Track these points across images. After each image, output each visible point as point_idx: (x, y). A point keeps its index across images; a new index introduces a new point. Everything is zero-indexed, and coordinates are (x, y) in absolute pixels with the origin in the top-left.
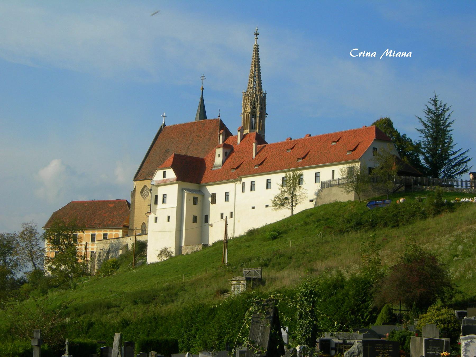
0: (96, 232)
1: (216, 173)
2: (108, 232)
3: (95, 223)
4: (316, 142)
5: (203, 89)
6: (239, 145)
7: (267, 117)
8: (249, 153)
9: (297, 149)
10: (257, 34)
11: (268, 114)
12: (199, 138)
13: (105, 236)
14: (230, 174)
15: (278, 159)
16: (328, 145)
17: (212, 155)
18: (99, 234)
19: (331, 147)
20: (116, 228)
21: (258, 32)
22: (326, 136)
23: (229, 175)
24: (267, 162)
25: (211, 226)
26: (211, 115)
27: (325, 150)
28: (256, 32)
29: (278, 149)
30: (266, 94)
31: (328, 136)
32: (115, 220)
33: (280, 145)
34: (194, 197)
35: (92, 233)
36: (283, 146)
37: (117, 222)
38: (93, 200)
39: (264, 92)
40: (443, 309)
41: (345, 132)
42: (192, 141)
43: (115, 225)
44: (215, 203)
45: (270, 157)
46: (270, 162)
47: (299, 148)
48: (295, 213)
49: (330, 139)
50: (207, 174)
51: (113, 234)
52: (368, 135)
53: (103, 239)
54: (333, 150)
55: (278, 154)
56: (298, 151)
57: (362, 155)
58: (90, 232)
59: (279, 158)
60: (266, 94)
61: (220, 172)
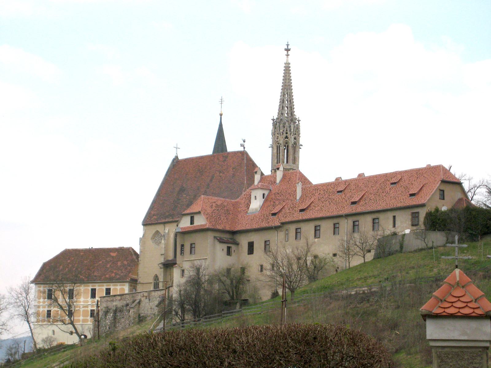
0: (97, 287)
1: (252, 218)
2: (112, 287)
3: (95, 276)
4: (372, 183)
5: (221, 115)
6: (279, 186)
7: (301, 148)
8: (292, 195)
9: (349, 190)
10: (288, 50)
11: (302, 145)
12: (221, 174)
13: (108, 291)
14: (270, 219)
15: (327, 202)
16: (386, 187)
17: (246, 197)
18: (101, 289)
19: (390, 189)
20: (121, 280)
21: (289, 48)
22: (384, 176)
23: (269, 221)
24: (314, 206)
25: (92, 248)
26: (232, 146)
27: (383, 192)
28: (286, 48)
29: (327, 190)
30: (300, 121)
31: (386, 176)
32: (119, 272)
33: (328, 186)
34: (248, 254)
35: (92, 288)
36: (332, 187)
37: (122, 274)
38: (91, 248)
39: (298, 119)
40: (22, 364)
41: (406, 172)
42: (213, 177)
43: (119, 278)
44: (253, 254)
45: (317, 200)
46: (318, 206)
47: (351, 189)
48: (351, 265)
49: (388, 180)
50: (241, 219)
51: (117, 289)
52: (433, 175)
53: (105, 295)
54: (393, 193)
55: (326, 197)
56: (350, 193)
57: (428, 199)
58: (89, 286)
59: (329, 202)
60: (300, 121)
61: (258, 217)
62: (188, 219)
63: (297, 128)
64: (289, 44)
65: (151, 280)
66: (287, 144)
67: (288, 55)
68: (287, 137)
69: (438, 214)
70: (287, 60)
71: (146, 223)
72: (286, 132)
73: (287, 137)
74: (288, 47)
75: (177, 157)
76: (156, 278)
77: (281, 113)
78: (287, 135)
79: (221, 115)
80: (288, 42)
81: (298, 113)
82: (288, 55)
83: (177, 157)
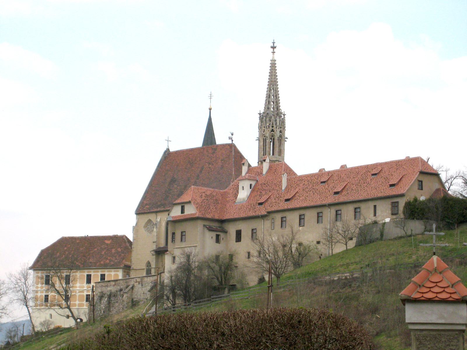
0: (92, 273)
1: (240, 208)
2: (106, 273)
3: (91, 263)
4: (354, 174)
5: (210, 109)
6: (265, 177)
7: (286, 141)
8: (277, 185)
9: (332, 181)
10: (274, 47)
11: (287, 138)
12: (210, 166)
13: (103, 277)
14: (257, 209)
15: (311, 192)
16: (368, 178)
17: (234, 187)
18: (96, 275)
19: (371, 180)
20: (115, 266)
21: (275, 45)
22: (365, 167)
23: (256, 210)
24: (299, 196)
25: (88, 235)
26: (221, 139)
27: (364, 183)
28: (272, 45)
29: (311, 181)
30: (286, 115)
31: (367, 168)
32: (114, 259)
33: (312, 177)
34: (236, 242)
35: (88, 274)
36: (316, 178)
37: (116, 261)
38: (86, 236)
39: (283, 113)
41: (386, 163)
42: (202, 168)
43: (113, 264)
44: (241, 241)
45: (302, 190)
46: (302, 196)
47: (334, 180)
48: (334, 252)
49: (369, 171)
50: (229, 208)
51: (111, 275)
52: (412, 167)
53: (99, 281)
54: (374, 183)
55: (310, 187)
56: (333, 183)
57: (407, 189)
58: (84, 272)
59: (313, 192)
60: (286, 115)
61: (245, 206)
62: (179, 208)
63: (283, 122)
64: (275, 42)
65: (144, 266)
66: (273, 137)
67: (274, 52)
68: (273, 131)
69: (417, 203)
70: (273, 57)
71: (139, 212)
72: (272, 125)
73: (273, 131)
74: (274, 44)
75: (168, 149)
76: (149, 264)
77: (267, 108)
78: (273, 128)
79: (210, 109)
80: (274, 40)
81: (283, 108)
82: (274, 52)
83: (168, 149)
